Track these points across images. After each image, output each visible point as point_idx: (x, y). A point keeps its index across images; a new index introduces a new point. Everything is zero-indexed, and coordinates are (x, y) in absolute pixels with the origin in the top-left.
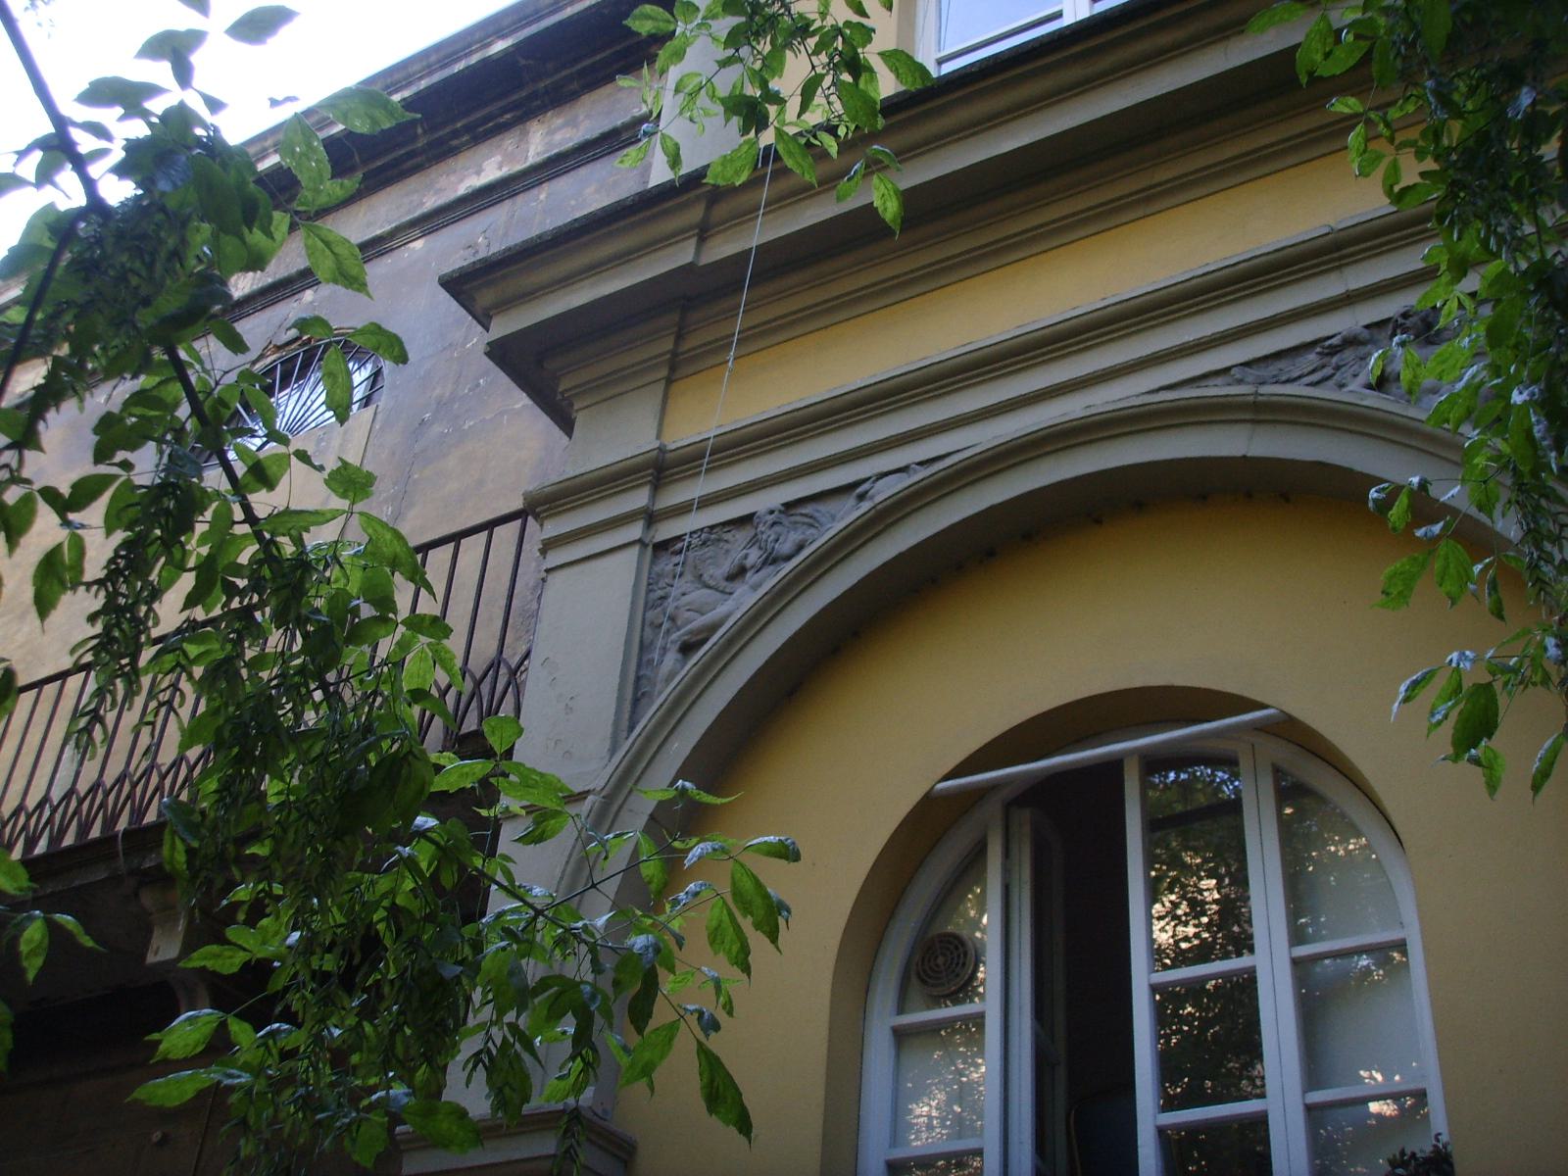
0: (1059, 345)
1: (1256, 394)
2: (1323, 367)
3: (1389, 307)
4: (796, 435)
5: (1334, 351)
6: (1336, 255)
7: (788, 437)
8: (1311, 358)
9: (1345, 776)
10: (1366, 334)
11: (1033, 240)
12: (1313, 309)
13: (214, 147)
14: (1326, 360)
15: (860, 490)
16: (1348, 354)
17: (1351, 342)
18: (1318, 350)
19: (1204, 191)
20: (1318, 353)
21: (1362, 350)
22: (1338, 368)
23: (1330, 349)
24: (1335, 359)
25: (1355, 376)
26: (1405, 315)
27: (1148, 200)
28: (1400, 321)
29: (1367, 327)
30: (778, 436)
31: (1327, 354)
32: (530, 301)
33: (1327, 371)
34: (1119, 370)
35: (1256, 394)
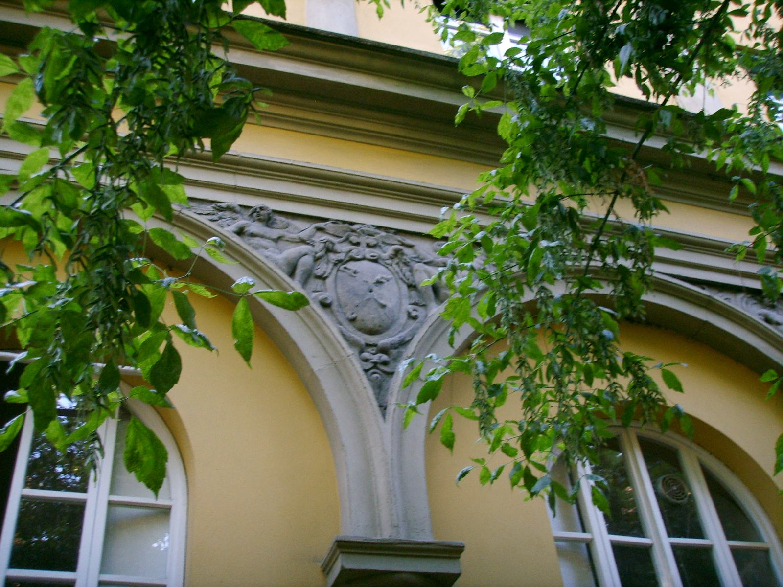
0: (443, 201)
1: (180, 212)
2: (214, 214)
3: (255, 202)
4: (425, 200)
5: (221, 209)
6: (235, 167)
7: (388, 193)
8: (209, 208)
9: (187, 481)
10: (238, 209)
11: (350, 133)
12: (276, 195)
13: (749, 49)
14: (215, 212)
15: (321, 225)
16: (227, 214)
17: (230, 209)
18: (213, 205)
19: (363, 140)
20: (214, 207)
21: (235, 215)
22: (221, 218)
23: (221, 208)
24: (220, 214)
25: (229, 225)
26: (261, 208)
27: (420, 145)
28: (258, 210)
29: (240, 206)
30: (431, 199)
31: (217, 210)
32: (388, 78)
33: (215, 217)
34: (406, 216)
35: (180, 212)
